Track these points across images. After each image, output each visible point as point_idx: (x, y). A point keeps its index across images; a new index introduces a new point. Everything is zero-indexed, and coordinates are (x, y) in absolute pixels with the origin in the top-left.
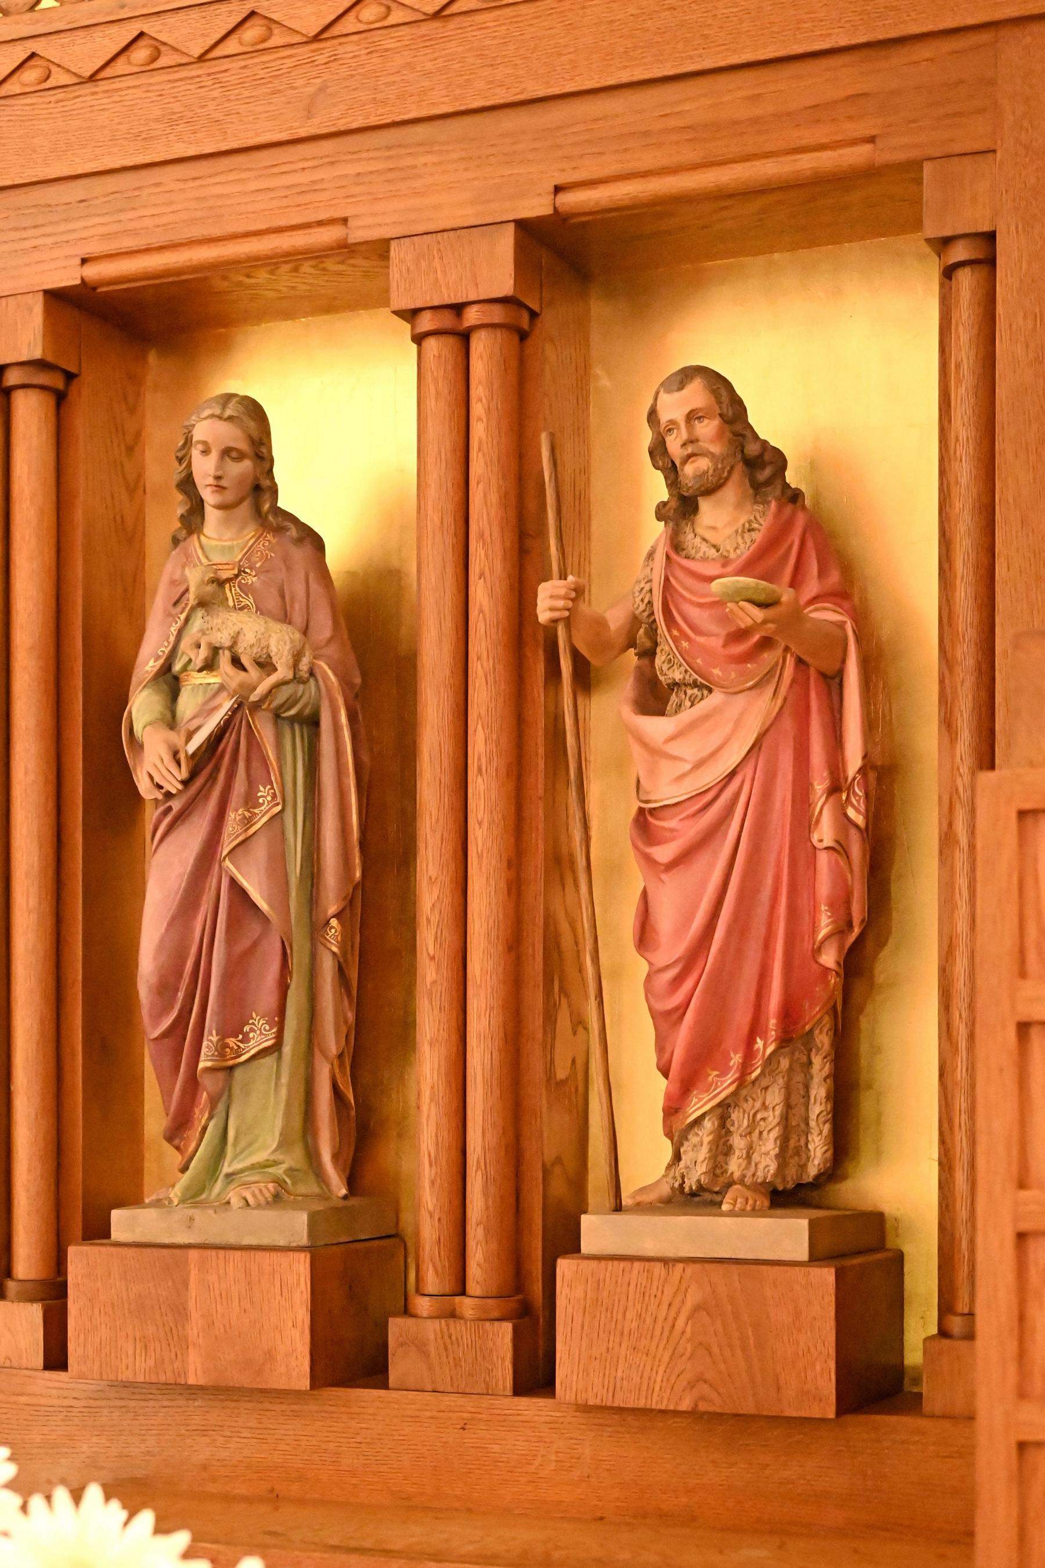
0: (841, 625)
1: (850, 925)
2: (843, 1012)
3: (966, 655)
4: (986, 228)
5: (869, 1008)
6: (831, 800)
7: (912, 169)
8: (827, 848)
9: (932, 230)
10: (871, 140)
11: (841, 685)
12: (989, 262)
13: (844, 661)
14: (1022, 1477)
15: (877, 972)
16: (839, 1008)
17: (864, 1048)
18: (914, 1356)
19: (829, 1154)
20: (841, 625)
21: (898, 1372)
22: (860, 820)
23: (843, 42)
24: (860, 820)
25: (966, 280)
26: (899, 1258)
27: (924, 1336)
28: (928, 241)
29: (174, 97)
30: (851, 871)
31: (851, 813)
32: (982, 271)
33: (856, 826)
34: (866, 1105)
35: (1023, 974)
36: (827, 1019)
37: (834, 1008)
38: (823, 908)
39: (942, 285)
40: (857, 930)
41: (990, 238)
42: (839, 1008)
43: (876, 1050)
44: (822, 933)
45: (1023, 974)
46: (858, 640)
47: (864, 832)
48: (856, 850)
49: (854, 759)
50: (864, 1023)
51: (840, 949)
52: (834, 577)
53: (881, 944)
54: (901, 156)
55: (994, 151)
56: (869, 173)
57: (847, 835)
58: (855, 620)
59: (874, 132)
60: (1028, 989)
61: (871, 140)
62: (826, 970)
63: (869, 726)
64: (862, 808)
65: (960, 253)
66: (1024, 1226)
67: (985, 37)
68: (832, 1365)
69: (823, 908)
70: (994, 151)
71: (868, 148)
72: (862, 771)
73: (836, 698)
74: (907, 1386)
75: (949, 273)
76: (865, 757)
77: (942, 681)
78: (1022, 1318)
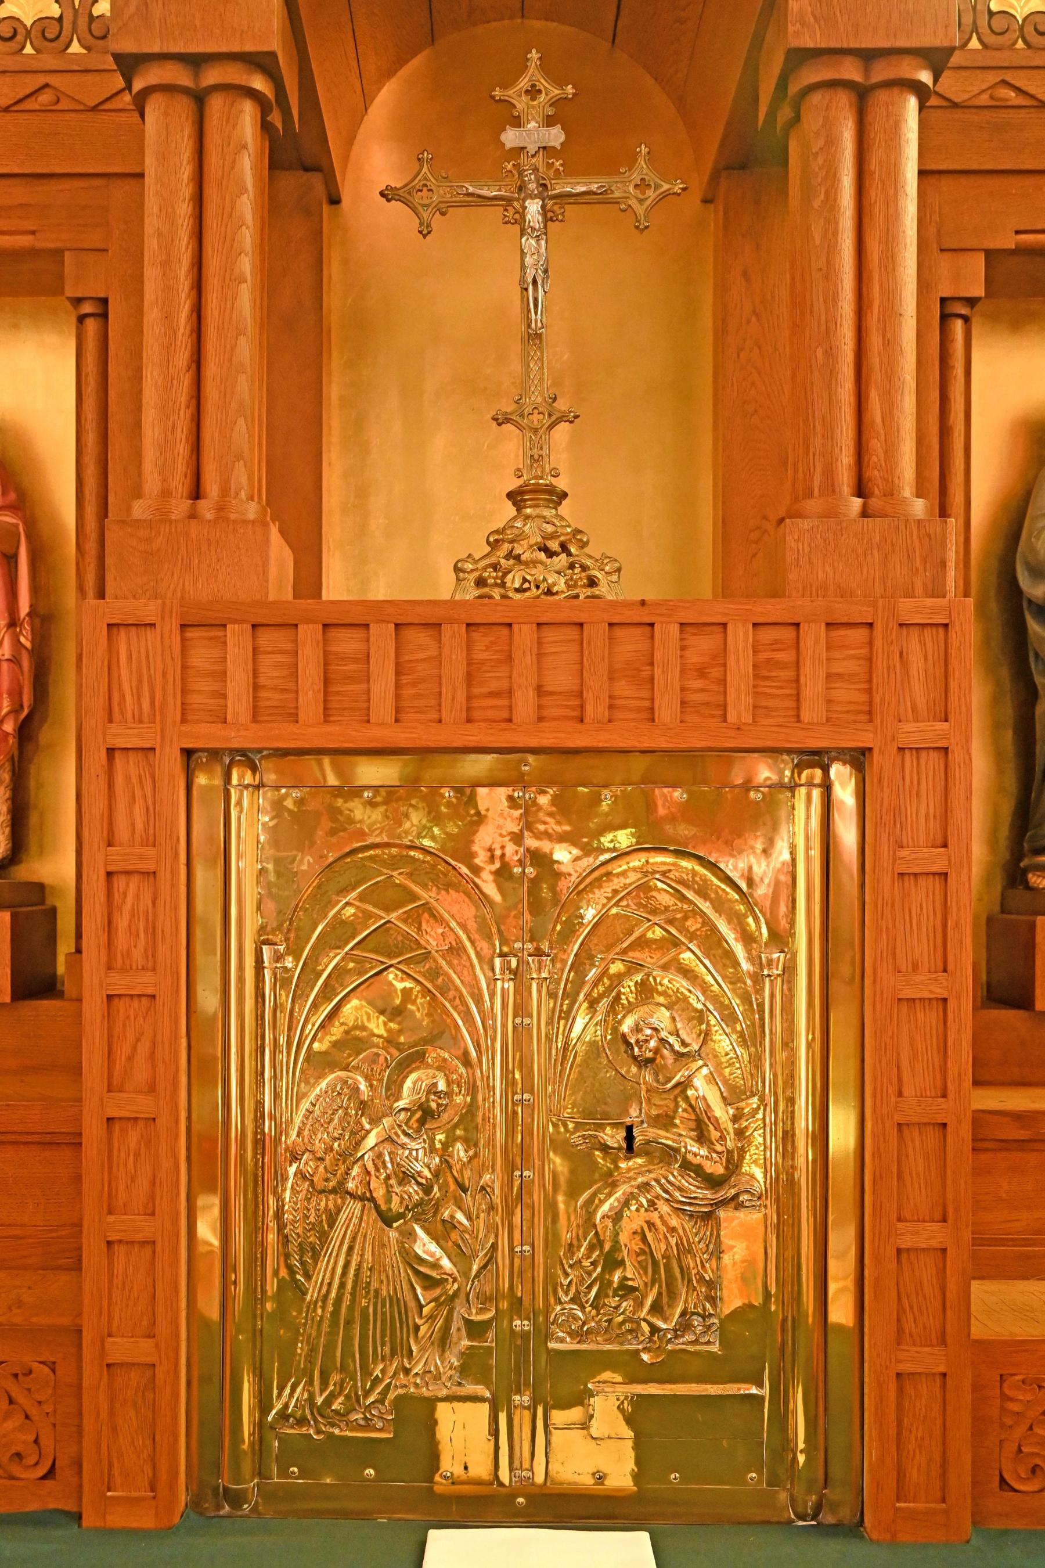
0: (16, 526)
1: (22, 706)
2: (19, 762)
3: (91, 547)
4: (102, 295)
5: (35, 761)
6: (11, 630)
7: (57, 254)
8: (7, 660)
9: (69, 292)
10: (33, 233)
11: (16, 562)
12: (104, 316)
13: (18, 547)
14: (109, 1015)
15: (40, 738)
16: (16, 759)
17: (32, 784)
18: (61, 969)
19: (10, 845)
20: (16, 526)
21: (54, 976)
22: (28, 645)
23: (16, 170)
24: (28, 645)
25: (92, 326)
26: (53, 911)
27: (67, 952)
28: (68, 298)
29: (521, 1273)
30: (23, 675)
31: (22, 639)
32: (99, 320)
33: (26, 648)
34: (33, 819)
35: (110, 721)
36: (7, 765)
37: (13, 757)
38: (5, 696)
39: (78, 328)
40: (26, 711)
41: (105, 301)
42: (16, 759)
43: (40, 786)
44: (5, 711)
45: (110, 721)
46: (28, 537)
47: (32, 652)
48: (26, 663)
49: (24, 608)
50: (33, 769)
51: (16, 720)
52: (12, 496)
53: (44, 720)
54: (51, 245)
55: (107, 250)
56: (34, 253)
57: (20, 654)
58: (25, 523)
59: (34, 228)
60: (114, 728)
61: (33, 233)
62: (8, 734)
63: (35, 589)
64: (30, 637)
65: (87, 308)
66: (110, 869)
67: (98, 182)
68: (9, 971)
69: (5, 696)
70: (106, 250)
71: (30, 238)
72: (29, 614)
73: (13, 570)
74: (59, 986)
75: (81, 319)
76: (31, 606)
77: (77, 564)
78: (110, 922)
